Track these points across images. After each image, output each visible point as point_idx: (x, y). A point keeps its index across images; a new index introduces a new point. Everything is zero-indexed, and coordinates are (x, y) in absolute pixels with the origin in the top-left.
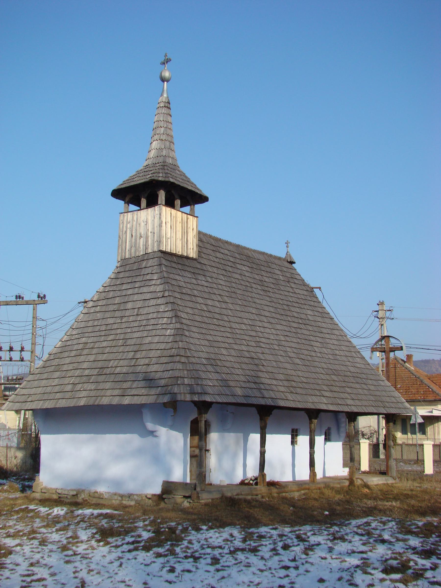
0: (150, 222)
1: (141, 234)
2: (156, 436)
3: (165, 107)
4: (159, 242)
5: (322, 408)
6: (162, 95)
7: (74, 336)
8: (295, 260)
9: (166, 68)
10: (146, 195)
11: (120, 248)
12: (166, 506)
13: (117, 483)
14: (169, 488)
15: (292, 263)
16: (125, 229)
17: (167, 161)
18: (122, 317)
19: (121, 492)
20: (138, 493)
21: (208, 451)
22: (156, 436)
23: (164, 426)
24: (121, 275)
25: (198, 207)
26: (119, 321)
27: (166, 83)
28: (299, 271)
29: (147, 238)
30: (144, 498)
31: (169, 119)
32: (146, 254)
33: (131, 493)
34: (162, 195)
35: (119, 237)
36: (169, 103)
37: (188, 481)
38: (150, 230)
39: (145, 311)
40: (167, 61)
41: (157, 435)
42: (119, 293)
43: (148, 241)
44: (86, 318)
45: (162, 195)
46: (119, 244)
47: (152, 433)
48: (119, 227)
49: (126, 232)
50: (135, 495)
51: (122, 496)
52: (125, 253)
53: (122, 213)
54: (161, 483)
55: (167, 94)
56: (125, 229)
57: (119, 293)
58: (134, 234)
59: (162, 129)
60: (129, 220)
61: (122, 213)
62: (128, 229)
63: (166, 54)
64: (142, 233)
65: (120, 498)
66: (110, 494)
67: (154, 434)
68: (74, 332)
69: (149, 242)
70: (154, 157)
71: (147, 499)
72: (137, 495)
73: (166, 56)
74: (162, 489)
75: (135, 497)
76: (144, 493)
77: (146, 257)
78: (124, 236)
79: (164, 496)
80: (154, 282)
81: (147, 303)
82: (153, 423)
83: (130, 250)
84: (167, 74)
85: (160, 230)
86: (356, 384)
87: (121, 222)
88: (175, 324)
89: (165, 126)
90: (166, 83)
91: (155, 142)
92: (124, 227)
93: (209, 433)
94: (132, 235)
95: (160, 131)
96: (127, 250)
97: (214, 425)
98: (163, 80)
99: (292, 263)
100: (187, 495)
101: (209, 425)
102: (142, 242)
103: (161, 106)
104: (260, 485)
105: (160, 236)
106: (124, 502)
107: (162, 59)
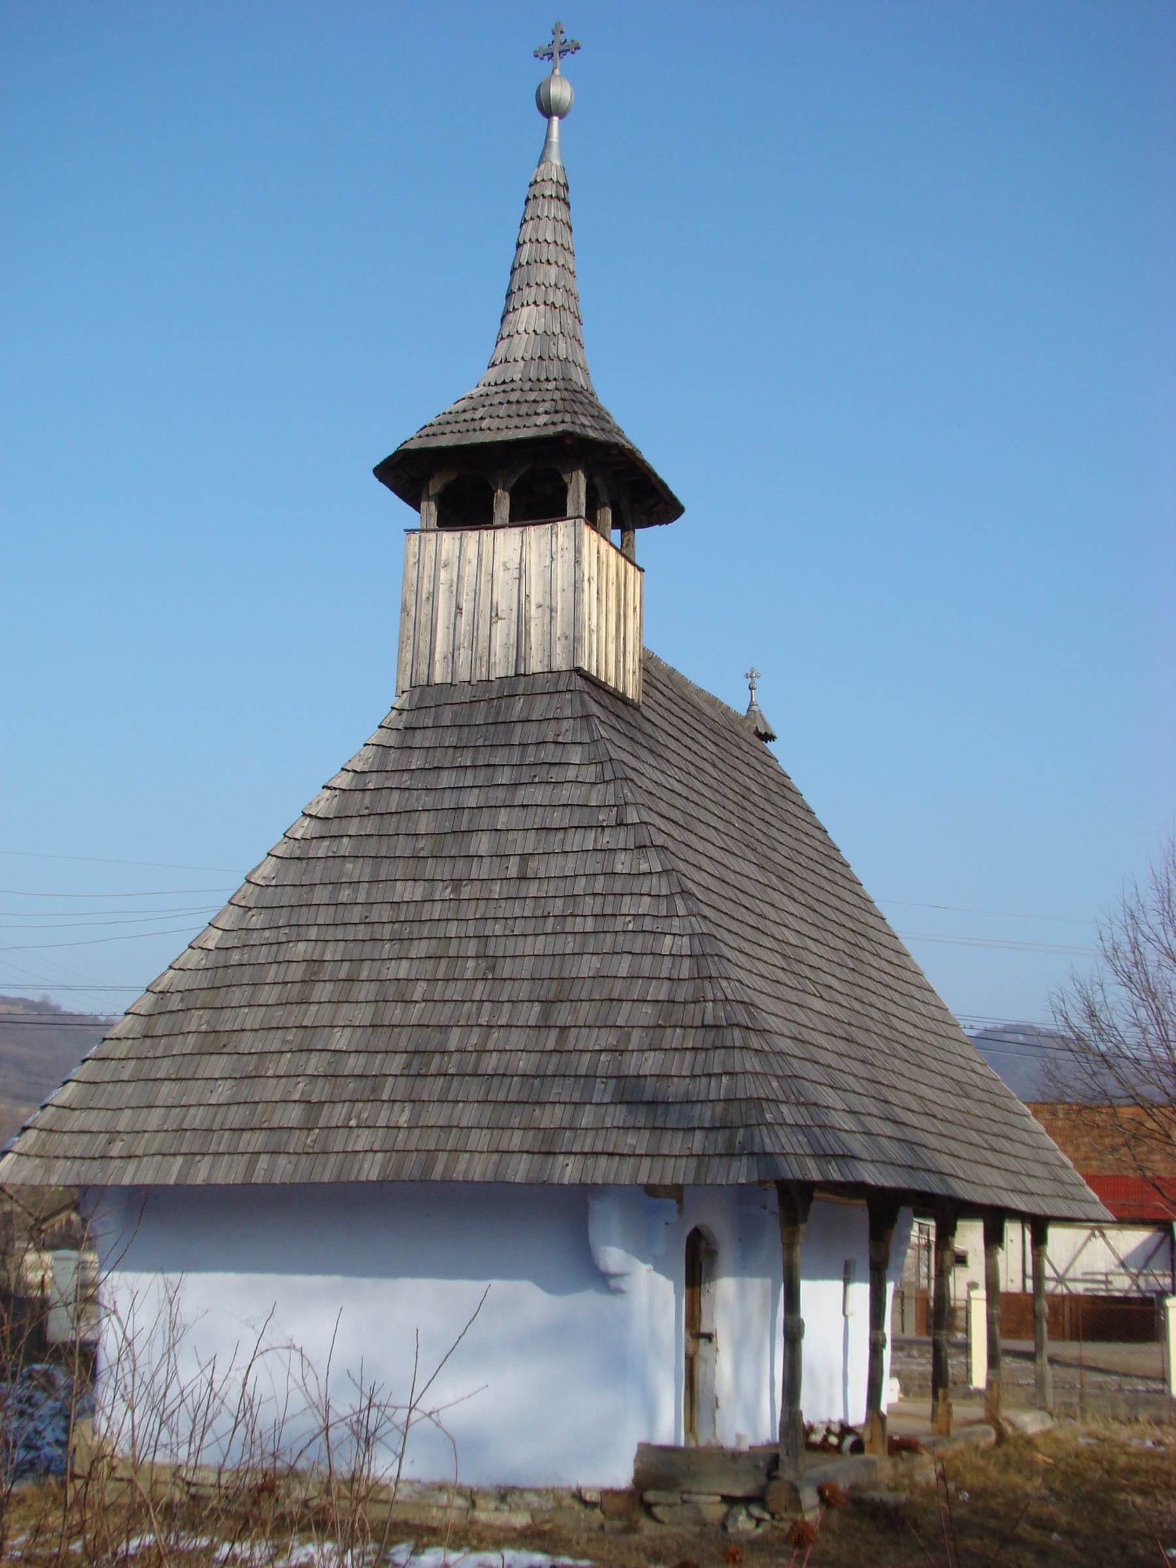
0: (534, 571)
1: (494, 608)
2: (620, 1291)
3: (558, 198)
4: (575, 642)
5: (1013, 1206)
6: (543, 159)
7: (255, 934)
8: (775, 730)
9: (557, 72)
10: (513, 481)
11: (410, 648)
12: (664, 1530)
13: (455, 1445)
14: (661, 1471)
15: (768, 737)
16: (426, 587)
17: (574, 378)
18: (457, 883)
19: (468, 1479)
20: (540, 1484)
21: (709, 1337)
22: (620, 1291)
23: (644, 1261)
24: (419, 739)
25: (644, 537)
26: (448, 894)
27: (556, 119)
28: (785, 764)
29: (522, 621)
30: (568, 1501)
31: (566, 239)
32: (517, 675)
33: (511, 1482)
34: (578, 486)
35: (405, 609)
36: (566, 186)
37: (682, 1443)
38: (535, 598)
39: (555, 866)
40: (559, 49)
41: (623, 1286)
42: (428, 800)
43: (528, 633)
44: (293, 874)
45: (578, 486)
46: (401, 635)
47: (604, 1281)
48: (405, 577)
49: (433, 596)
50: (530, 1490)
51: (472, 1497)
52: (430, 665)
53: (413, 531)
54: (630, 1452)
55: (562, 160)
56: (426, 587)
57: (428, 800)
58: (466, 606)
59: (553, 271)
60: (444, 557)
61: (413, 531)
62: (442, 588)
63: (558, 25)
64: (503, 606)
65: (460, 1502)
66: (417, 1487)
67: (613, 1283)
68: (256, 920)
69: (533, 639)
70: (528, 357)
71: (578, 1507)
72: (537, 1491)
73: (557, 31)
74: (637, 1472)
75: (531, 1498)
76: (565, 1484)
77: (519, 683)
78: (426, 609)
79: (650, 1496)
80: (571, 773)
81: (555, 842)
82: (627, 1250)
83: (452, 657)
84: (560, 91)
85: (577, 603)
86: (923, 1118)
87: (412, 560)
88: (686, 921)
89: (561, 263)
90: (556, 119)
91: (526, 310)
92: (426, 580)
93: (712, 1277)
94: (459, 609)
95: (546, 274)
96: (438, 656)
97: (727, 1254)
98: (547, 109)
99: (768, 737)
100: (738, 1492)
101: (713, 1254)
102: (503, 633)
103: (547, 193)
104: (873, 1451)
105: (576, 621)
106: (482, 1516)
107: (544, 40)
